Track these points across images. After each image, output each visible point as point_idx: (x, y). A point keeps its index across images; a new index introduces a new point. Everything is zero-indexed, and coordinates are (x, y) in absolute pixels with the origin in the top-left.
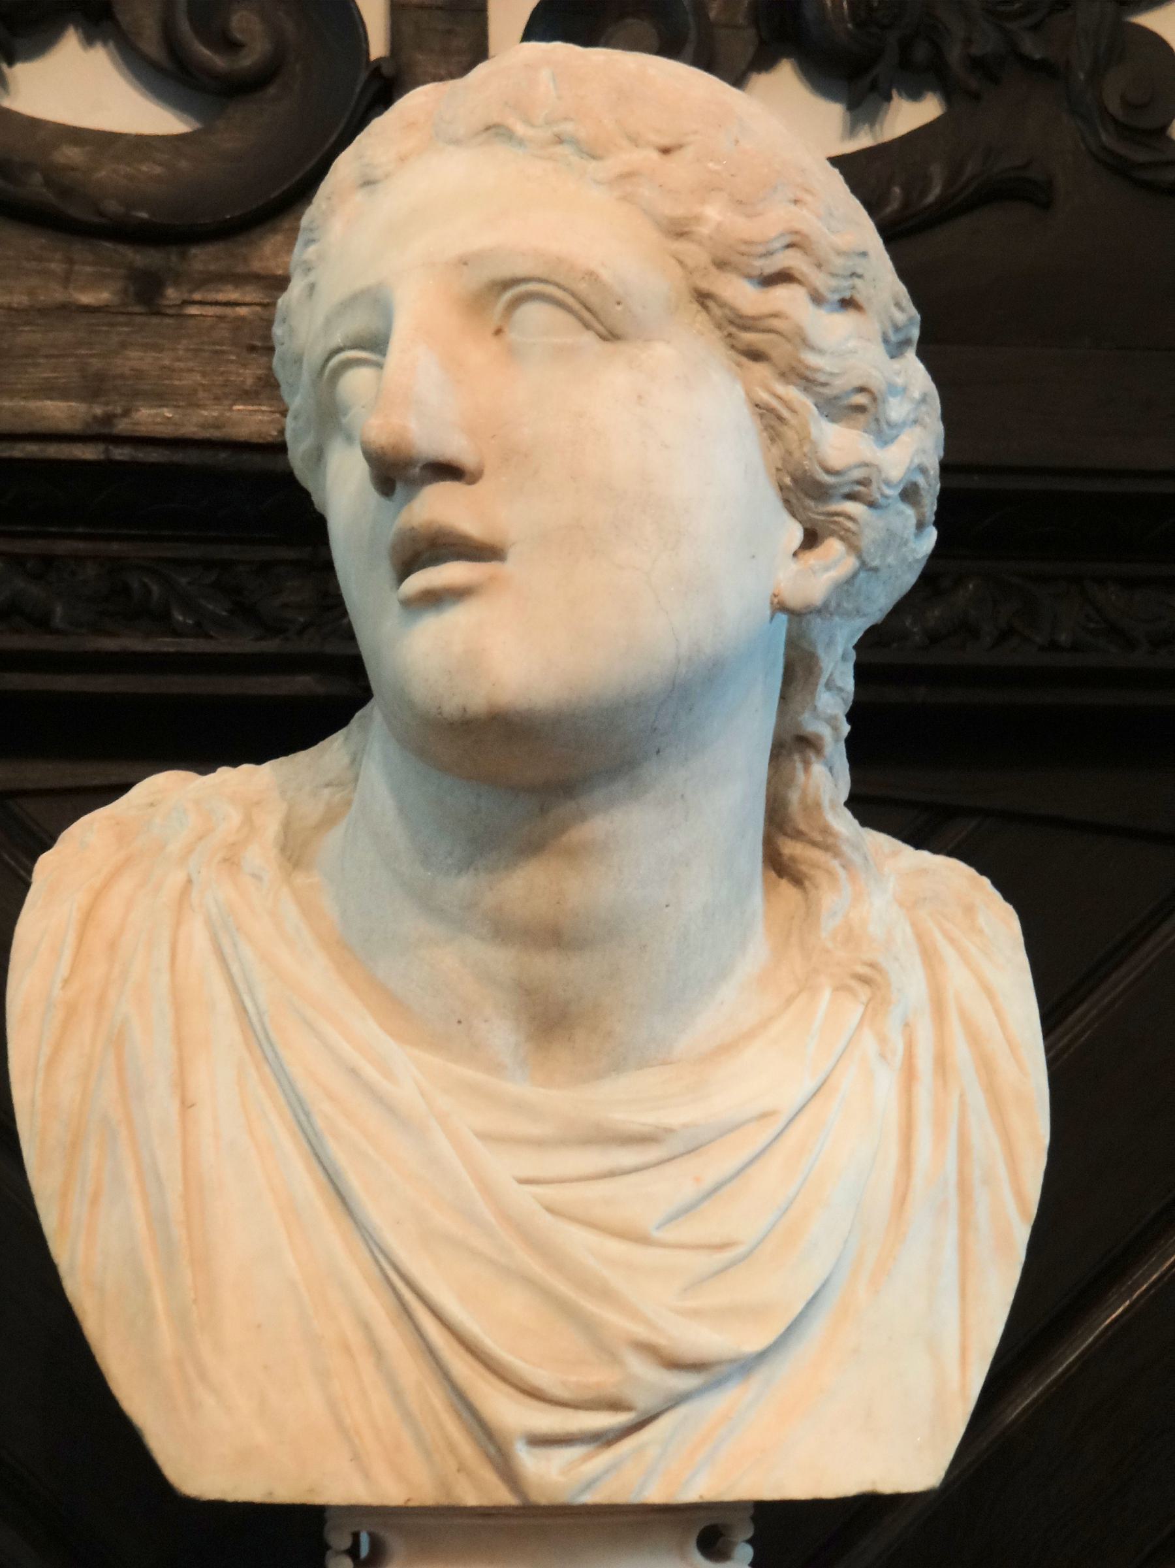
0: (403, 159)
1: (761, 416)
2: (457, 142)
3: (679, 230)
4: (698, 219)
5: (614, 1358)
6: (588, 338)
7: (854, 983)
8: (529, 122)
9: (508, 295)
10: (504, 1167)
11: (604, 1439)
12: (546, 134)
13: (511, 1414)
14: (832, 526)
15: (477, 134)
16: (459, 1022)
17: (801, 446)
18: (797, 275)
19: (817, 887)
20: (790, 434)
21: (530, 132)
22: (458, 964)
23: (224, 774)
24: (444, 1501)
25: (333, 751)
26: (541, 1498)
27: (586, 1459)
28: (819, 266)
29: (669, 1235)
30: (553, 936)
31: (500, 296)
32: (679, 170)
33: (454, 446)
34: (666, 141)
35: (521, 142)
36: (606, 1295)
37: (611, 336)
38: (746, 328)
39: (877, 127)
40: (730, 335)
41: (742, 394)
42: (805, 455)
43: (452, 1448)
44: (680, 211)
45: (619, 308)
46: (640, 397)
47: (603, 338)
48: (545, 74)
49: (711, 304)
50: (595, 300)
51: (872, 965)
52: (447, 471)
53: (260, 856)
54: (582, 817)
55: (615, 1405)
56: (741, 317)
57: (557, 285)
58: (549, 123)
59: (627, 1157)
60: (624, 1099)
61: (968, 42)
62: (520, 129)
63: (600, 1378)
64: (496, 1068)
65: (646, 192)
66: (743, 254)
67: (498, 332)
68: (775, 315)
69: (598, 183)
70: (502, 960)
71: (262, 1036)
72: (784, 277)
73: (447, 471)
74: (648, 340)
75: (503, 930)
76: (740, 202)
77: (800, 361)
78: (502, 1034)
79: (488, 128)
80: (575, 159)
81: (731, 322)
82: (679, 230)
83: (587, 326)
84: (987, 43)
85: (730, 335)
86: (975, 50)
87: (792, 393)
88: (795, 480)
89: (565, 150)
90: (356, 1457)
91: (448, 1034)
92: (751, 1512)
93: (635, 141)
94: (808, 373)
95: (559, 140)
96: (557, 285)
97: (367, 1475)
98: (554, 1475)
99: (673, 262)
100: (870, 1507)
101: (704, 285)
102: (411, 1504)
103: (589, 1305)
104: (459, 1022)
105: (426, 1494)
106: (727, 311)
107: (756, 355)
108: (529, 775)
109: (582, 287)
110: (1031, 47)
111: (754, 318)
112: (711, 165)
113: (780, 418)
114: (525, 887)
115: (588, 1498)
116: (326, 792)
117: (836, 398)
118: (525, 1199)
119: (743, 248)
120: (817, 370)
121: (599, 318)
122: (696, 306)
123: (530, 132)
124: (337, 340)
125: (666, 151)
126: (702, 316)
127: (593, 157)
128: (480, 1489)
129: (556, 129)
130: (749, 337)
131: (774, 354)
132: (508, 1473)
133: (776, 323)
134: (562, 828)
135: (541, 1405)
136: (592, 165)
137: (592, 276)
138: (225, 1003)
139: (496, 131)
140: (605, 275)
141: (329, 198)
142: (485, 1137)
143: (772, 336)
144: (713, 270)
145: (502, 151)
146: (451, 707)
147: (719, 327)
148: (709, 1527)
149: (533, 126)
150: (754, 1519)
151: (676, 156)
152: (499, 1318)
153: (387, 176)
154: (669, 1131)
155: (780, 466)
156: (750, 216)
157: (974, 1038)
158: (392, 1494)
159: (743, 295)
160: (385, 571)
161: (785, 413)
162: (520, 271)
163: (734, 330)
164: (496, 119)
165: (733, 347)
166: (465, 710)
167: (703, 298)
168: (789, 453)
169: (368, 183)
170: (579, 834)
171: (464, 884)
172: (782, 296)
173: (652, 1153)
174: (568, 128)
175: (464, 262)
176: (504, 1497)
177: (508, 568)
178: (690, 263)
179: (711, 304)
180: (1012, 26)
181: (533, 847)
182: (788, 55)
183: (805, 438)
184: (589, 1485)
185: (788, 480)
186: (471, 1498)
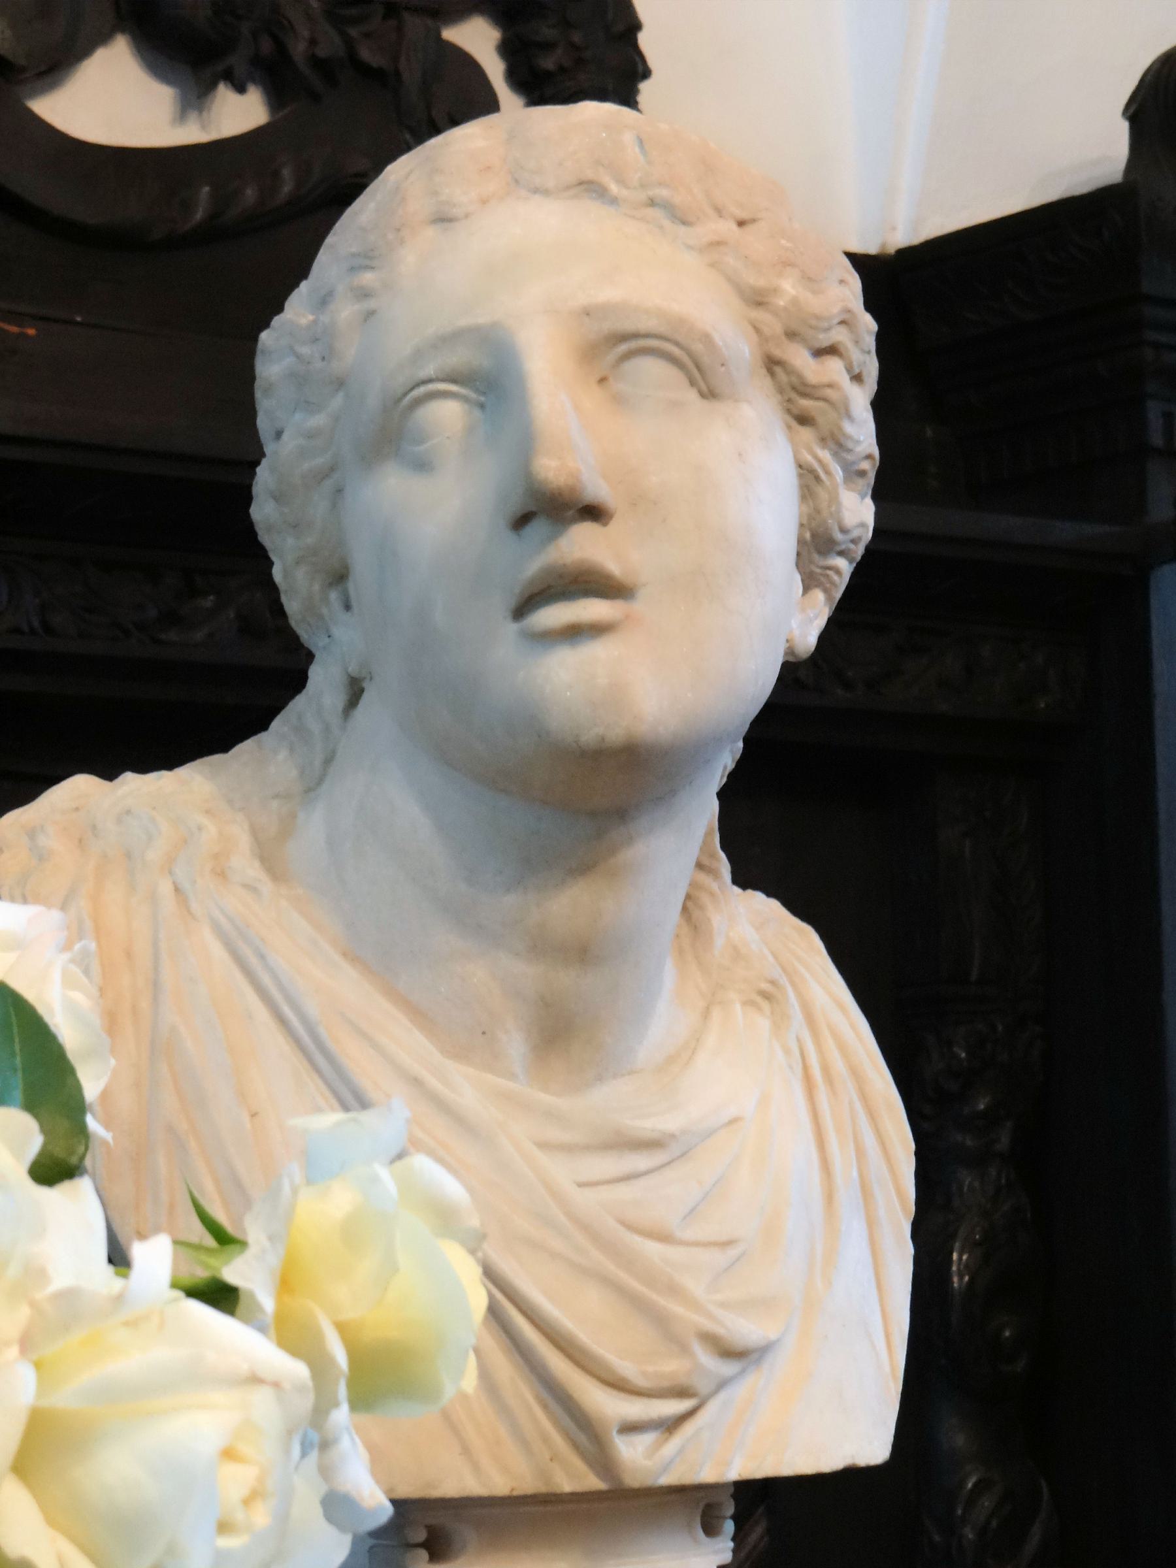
0: (484, 202)
1: (800, 476)
2: (545, 192)
3: (758, 299)
4: (776, 291)
5: (685, 1349)
6: (692, 395)
7: (759, 999)
8: (621, 182)
9: (623, 348)
10: (562, 1172)
11: (671, 1425)
12: (642, 196)
13: (609, 1406)
14: (822, 579)
15: (568, 188)
16: (484, 1033)
17: (829, 507)
18: (842, 349)
19: (702, 908)
20: (823, 495)
21: (625, 193)
22: (488, 977)
23: (130, 780)
24: (542, 1488)
25: (259, 763)
26: (633, 1480)
27: (658, 1446)
28: (857, 342)
29: (689, 1234)
30: (582, 952)
31: (616, 347)
32: (755, 242)
33: (597, 489)
34: (743, 215)
35: (614, 201)
36: (674, 1290)
37: (710, 394)
38: (804, 395)
39: (205, 114)
40: (789, 400)
41: (791, 455)
42: (831, 514)
43: (546, 1439)
44: (761, 282)
45: (723, 369)
46: (740, 455)
47: (702, 395)
48: (628, 138)
49: (778, 370)
50: (706, 360)
51: (773, 982)
52: (593, 513)
53: (244, 864)
54: (630, 840)
55: (681, 1392)
56: (805, 384)
57: (677, 344)
58: (643, 186)
59: (640, 1161)
60: (614, 1101)
61: (313, 42)
62: (614, 188)
63: (671, 1367)
64: (512, 1076)
65: (730, 260)
66: (811, 327)
67: (602, 380)
68: (830, 386)
69: (690, 247)
70: (528, 973)
71: (311, 1047)
72: (832, 350)
73: (593, 513)
74: (736, 401)
75: (546, 947)
76: (810, 279)
77: (840, 429)
78: (515, 1045)
79: (581, 183)
80: (666, 223)
81: (794, 388)
82: (758, 299)
83: (693, 383)
84: (330, 45)
85: (789, 400)
86: (322, 52)
87: (825, 455)
88: (813, 536)
89: (656, 213)
90: (466, 1451)
91: (471, 1043)
92: (732, 1490)
93: (719, 212)
94: (842, 440)
95: (652, 203)
96: (677, 344)
97: (476, 1467)
98: (643, 1459)
99: (750, 328)
100: (851, 1475)
101: (777, 353)
102: (515, 1493)
103: (663, 1301)
104: (484, 1033)
105: (528, 1484)
106: (794, 379)
107: (804, 420)
108: (581, 795)
109: (698, 347)
110: (366, 54)
111: (814, 387)
112: (783, 242)
113: (817, 478)
114: (567, 905)
115: (665, 1480)
116: (275, 804)
117: (854, 463)
118: (586, 1200)
119: (814, 322)
120: (849, 437)
121: (702, 376)
122: (764, 371)
123: (625, 193)
124: (430, 370)
125: (741, 223)
126: (768, 382)
127: (684, 223)
128: (574, 1477)
129: (651, 193)
130: (805, 403)
131: (820, 420)
132: (599, 1456)
133: (829, 393)
134: (613, 851)
135: (622, 1395)
136: (682, 229)
137: (707, 339)
138: (261, 1013)
139: (590, 188)
140: (717, 338)
141: (399, 230)
142: (544, 1146)
143: (821, 404)
144: (783, 338)
145: (593, 208)
146: (589, 737)
147: (781, 390)
148: (699, 1505)
149: (627, 187)
150: (735, 1496)
151: (749, 228)
152: (582, 1312)
153: (467, 216)
154: (673, 1136)
155: (805, 522)
156: (815, 292)
157: (843, 1048)
158: (499, 1484)
159: (800, 359)
160: (500, 603)
161: (823, 475)
162: (629, 326)
163: (794, 395)
164: (589, 174)
165: (789, 411)
166: (603, 739)
167: (772, 364)
168: (818, 511)
169: (443, 219)
170: (628, 855)
171: (511, 900)
172: (834, 369)
173: (658, 1158)
174: (664, 193)
175: (587, 312)
176: (593, 1482)
177: (638, 606)
178: (767, 331)
179: (778, 370)
180: (353, 32)
181: (583, 868)
182: (123, 31)
183: (834, 499)
184: (665, 1468)
185: (808, 535)
186: (567, 1487)
